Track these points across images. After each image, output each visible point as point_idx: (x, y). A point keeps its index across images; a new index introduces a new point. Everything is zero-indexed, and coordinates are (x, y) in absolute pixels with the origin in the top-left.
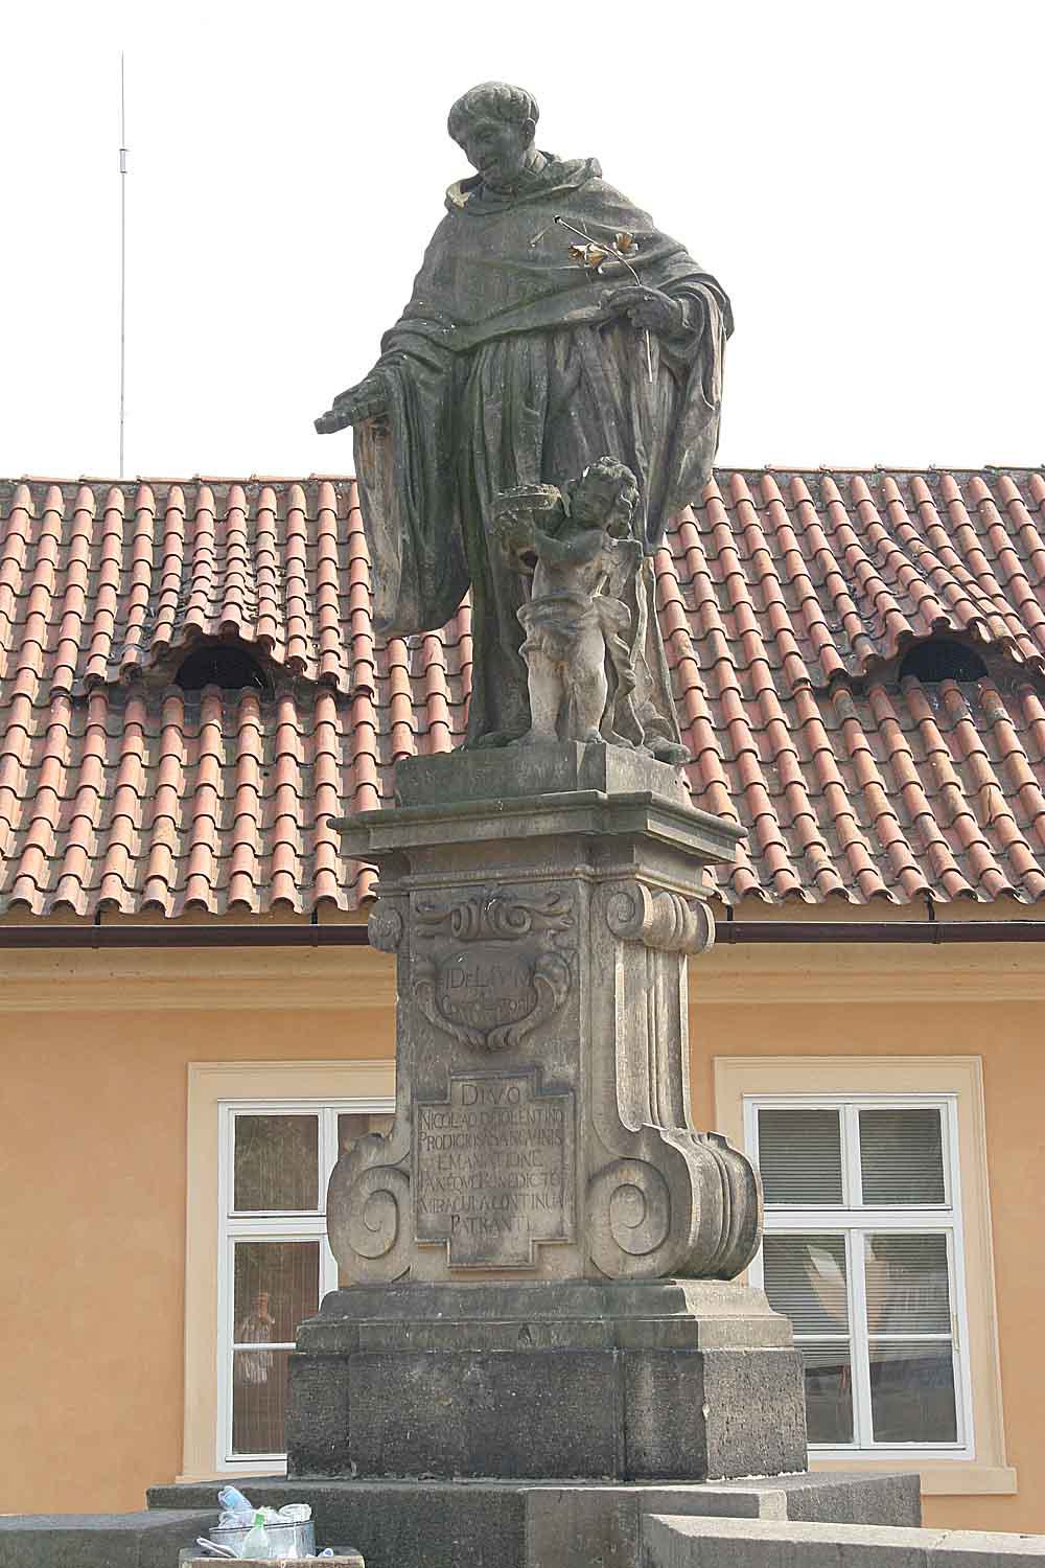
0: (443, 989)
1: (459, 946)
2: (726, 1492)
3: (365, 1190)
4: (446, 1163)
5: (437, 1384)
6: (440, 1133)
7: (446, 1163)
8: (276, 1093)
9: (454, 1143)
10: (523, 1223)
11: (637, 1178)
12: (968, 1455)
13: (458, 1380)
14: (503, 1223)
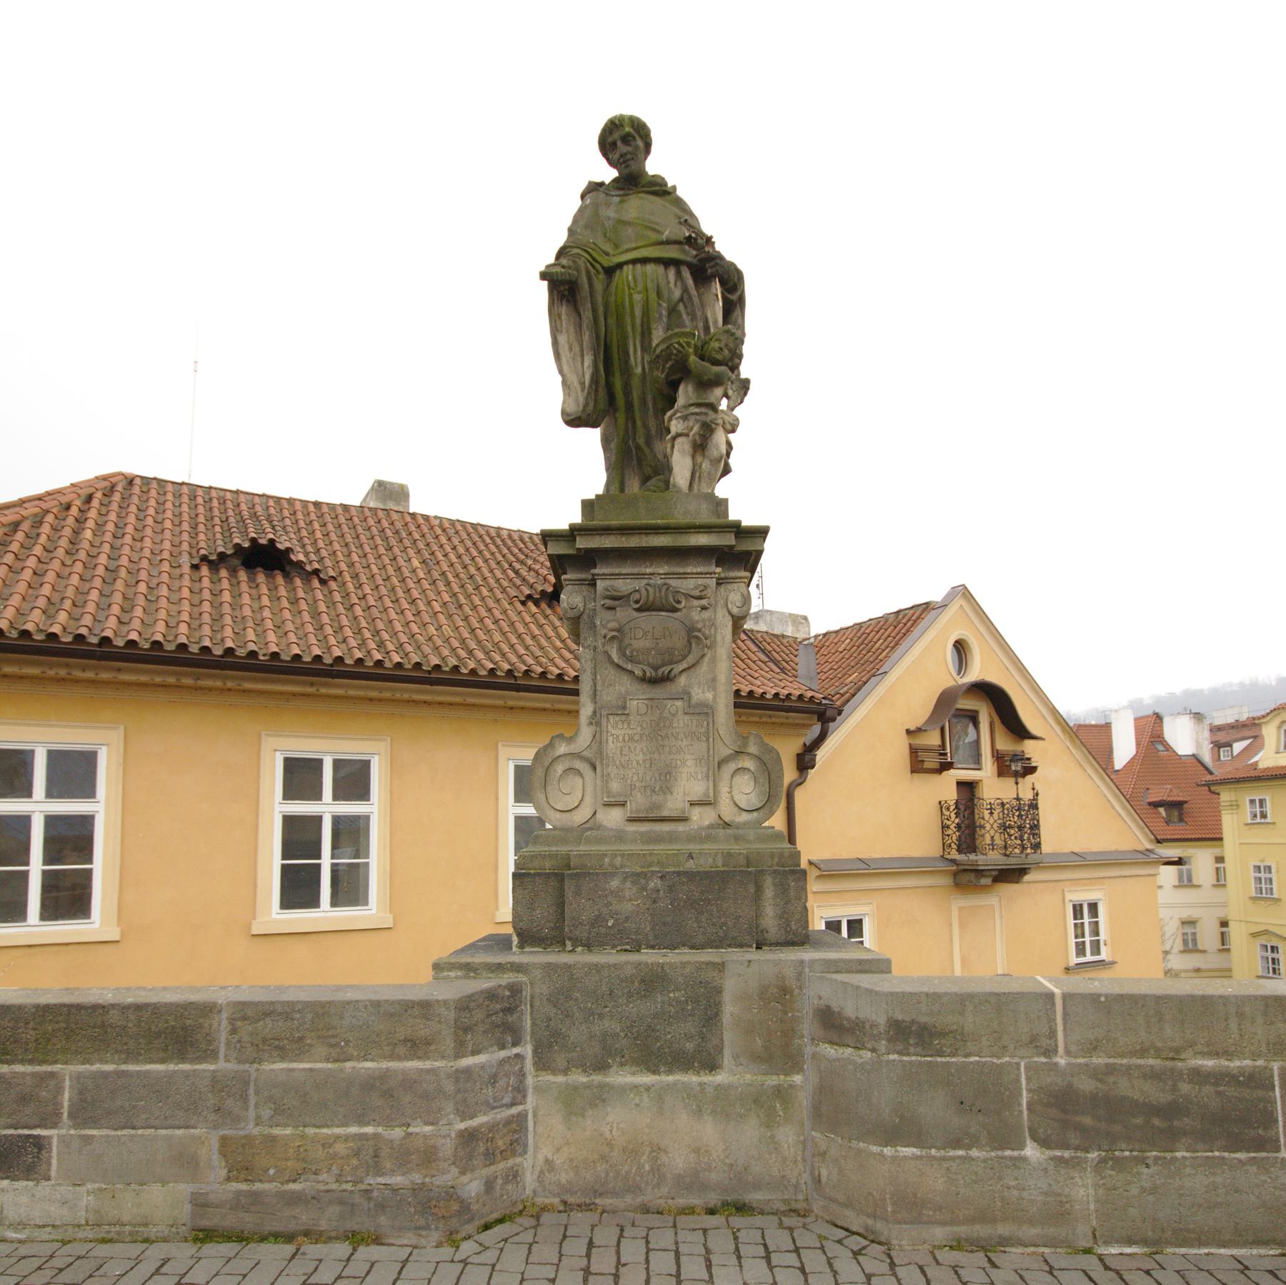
0: (626, 641)
1: (635, 614)
2: (1210, 991)
3: (559, 768)
4: (626, 751)
5: (629, 890)
6: (622, 732)
7: (626, 751)
8: (304, 747)
9: (631, 739)
10: (681, 790)
11: (749, 764)
12: (374, 912)
13: (644, 889)
14: (667, 790)
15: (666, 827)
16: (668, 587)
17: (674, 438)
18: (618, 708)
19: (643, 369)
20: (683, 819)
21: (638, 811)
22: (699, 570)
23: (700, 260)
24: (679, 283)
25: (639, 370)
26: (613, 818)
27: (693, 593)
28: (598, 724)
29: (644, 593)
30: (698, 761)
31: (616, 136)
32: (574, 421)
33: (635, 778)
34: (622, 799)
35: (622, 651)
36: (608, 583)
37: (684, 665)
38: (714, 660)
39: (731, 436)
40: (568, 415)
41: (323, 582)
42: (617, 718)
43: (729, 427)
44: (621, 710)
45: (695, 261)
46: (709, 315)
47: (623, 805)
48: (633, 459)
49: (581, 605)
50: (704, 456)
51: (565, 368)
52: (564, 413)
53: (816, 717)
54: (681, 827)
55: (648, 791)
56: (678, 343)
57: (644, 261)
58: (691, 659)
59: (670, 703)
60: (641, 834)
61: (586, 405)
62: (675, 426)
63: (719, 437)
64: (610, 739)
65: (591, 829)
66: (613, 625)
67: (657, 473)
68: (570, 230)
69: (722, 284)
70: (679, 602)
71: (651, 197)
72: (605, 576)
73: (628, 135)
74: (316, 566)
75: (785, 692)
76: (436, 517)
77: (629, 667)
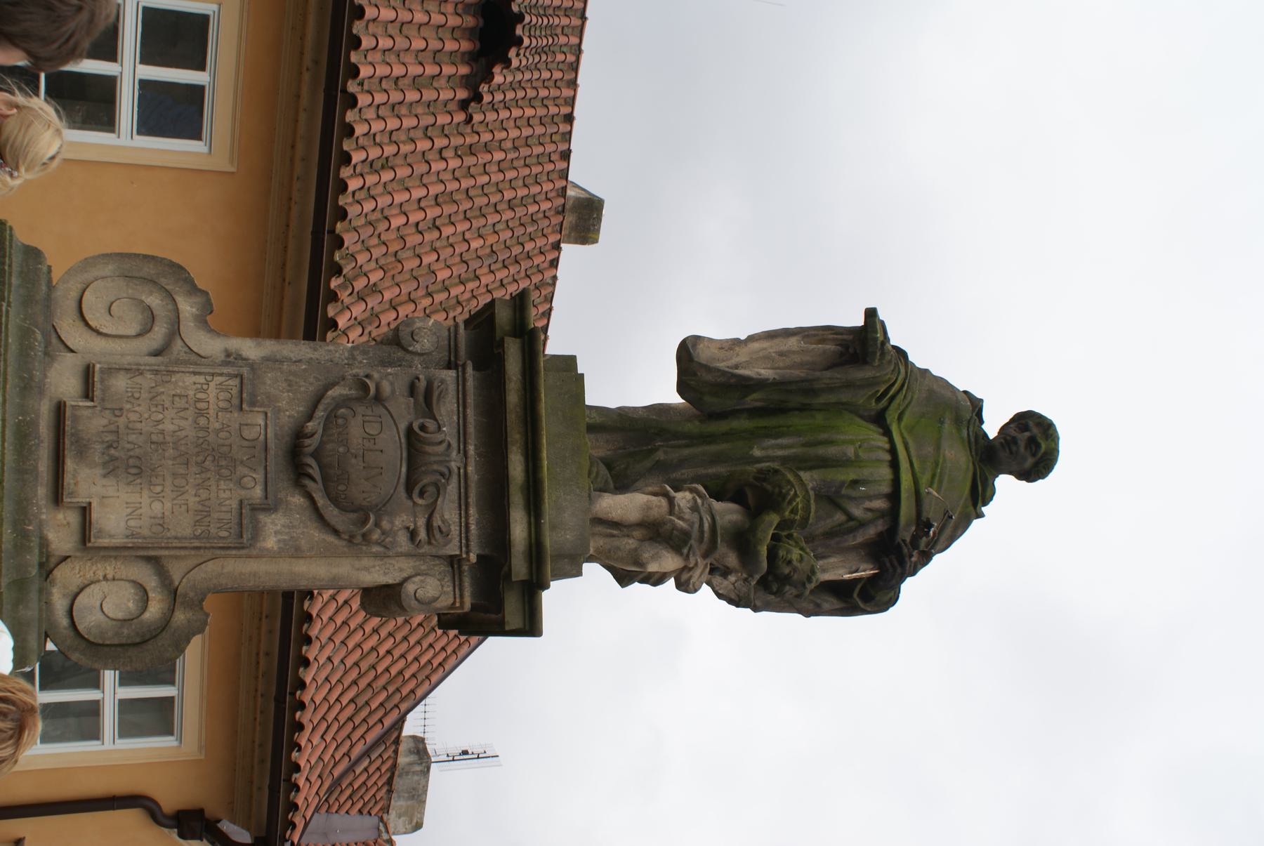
0: (360, 409)
1: (403, 426)
3: (154, 301)
4: (180, 403)
6: (212, 400)
7: (180, 403)
8: (224, 45)
9: (200, 413)
11: (155, 610)
14: (112, 468)
15: (44, 466)
16: (447, 476)
17: (666, 495)
18: (253, 395)
19: (759, 460)
20: (57, 497)
21: (76, 419)
22: (473, 527)
23: (899, 546)
24: (870, 515)
25: (757, 452)
26: (63, 381)
27: (437, 516)
28: (225, 363)
29: (440, 437)
30: (161, 522)
31: (1035, 431)
32: (687, 353)
33: (133, 417)
34: (97, 393)
35: (345, 402)
36: (452, 387)
37: (321, 501)
38: (327, 553)
39: (671, 582)
40: (694, 345)
41: (464, 105)
42: (235, 391)
43: (684, 577)
44: (245, 399)
45: (899, 540)
46: (832, 560)
47: (88, 394)
48: (635, 441)
49: (418, 347)
50: (642, 540)
51: (756, 346)
52: (696, 339)
53: (263, 834)
54: (42, 492)
55: (109, 438)
56: (796, 495)
57: (894, 465)
58: (332, 513)
59: (259, 476)
60: (34, 424)
61: (708, 368)
62: (683, 498)
63: (670, 562)
64: (201, 379)
65: (48, 344)
66: (386, 388)
67: (616, 478)
68: (926, 371)
69: (872, 579)
70: (422, 494)
71: (970, 475)
72: (461, 382)
73: (1038, 446)
74: (487, 98)
75: (301, 783)
76: (555, 278)
77: (320, 413)
